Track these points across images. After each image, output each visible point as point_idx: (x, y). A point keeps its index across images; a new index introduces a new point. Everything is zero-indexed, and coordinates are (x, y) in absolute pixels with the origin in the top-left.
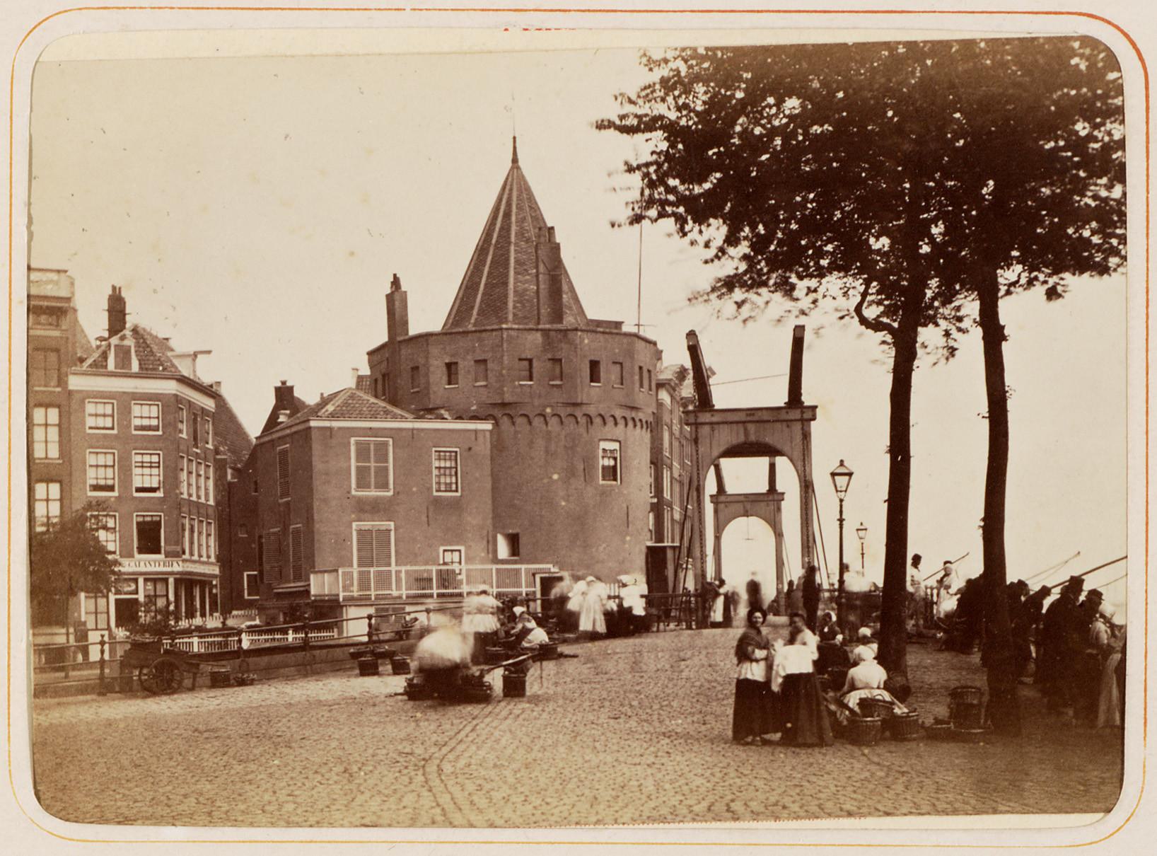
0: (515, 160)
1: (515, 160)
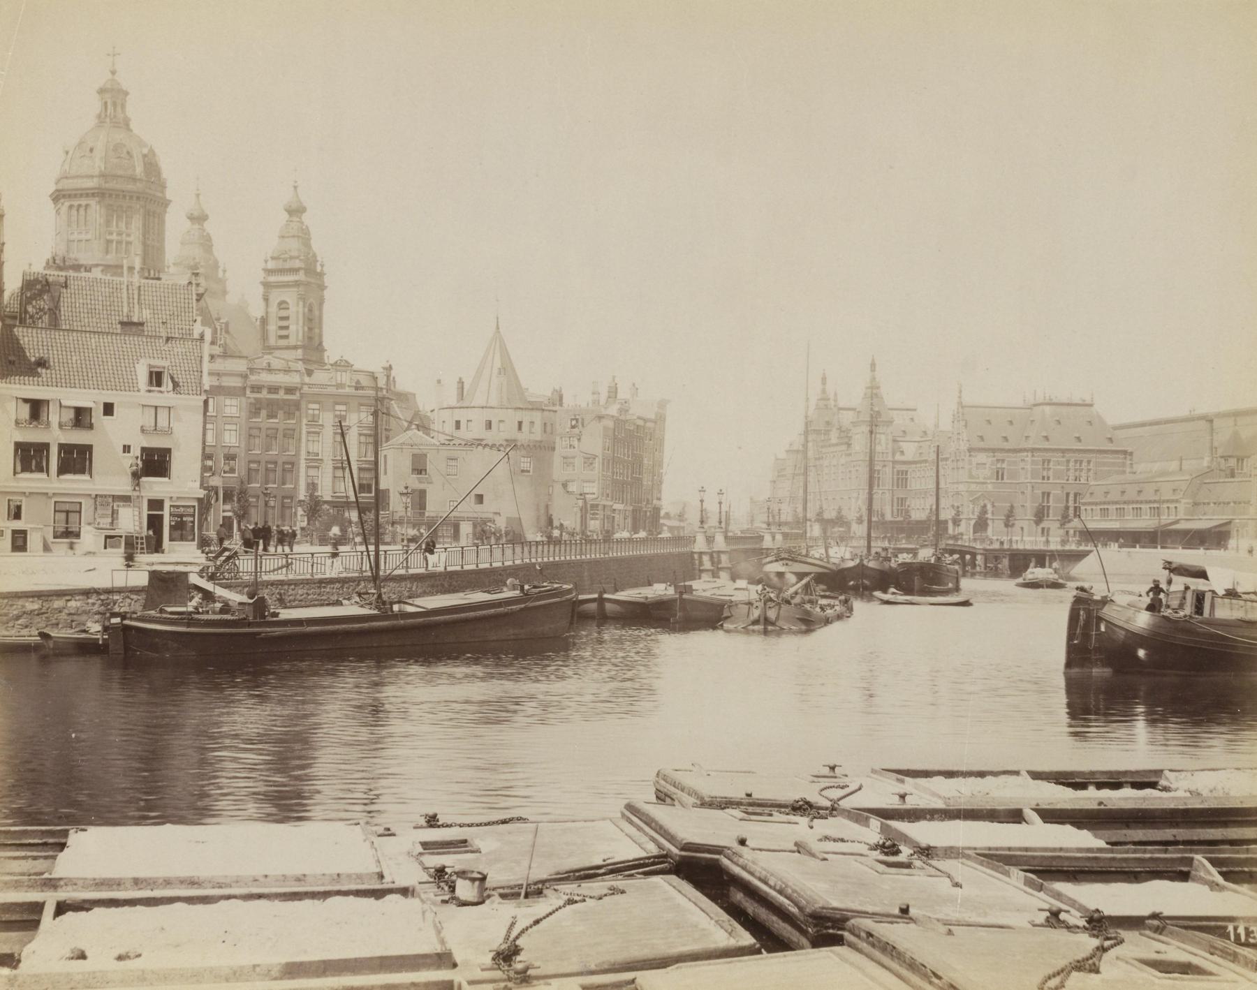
1: (498, 328)
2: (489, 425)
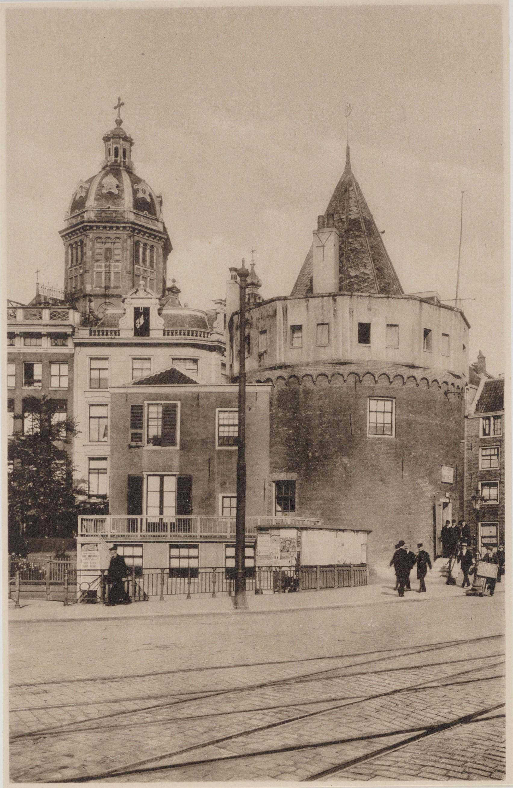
0: (348, 163)
1: (348, 163)
2: (364, 333)
